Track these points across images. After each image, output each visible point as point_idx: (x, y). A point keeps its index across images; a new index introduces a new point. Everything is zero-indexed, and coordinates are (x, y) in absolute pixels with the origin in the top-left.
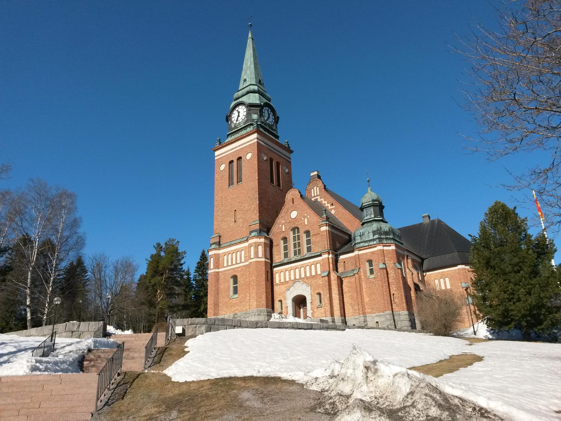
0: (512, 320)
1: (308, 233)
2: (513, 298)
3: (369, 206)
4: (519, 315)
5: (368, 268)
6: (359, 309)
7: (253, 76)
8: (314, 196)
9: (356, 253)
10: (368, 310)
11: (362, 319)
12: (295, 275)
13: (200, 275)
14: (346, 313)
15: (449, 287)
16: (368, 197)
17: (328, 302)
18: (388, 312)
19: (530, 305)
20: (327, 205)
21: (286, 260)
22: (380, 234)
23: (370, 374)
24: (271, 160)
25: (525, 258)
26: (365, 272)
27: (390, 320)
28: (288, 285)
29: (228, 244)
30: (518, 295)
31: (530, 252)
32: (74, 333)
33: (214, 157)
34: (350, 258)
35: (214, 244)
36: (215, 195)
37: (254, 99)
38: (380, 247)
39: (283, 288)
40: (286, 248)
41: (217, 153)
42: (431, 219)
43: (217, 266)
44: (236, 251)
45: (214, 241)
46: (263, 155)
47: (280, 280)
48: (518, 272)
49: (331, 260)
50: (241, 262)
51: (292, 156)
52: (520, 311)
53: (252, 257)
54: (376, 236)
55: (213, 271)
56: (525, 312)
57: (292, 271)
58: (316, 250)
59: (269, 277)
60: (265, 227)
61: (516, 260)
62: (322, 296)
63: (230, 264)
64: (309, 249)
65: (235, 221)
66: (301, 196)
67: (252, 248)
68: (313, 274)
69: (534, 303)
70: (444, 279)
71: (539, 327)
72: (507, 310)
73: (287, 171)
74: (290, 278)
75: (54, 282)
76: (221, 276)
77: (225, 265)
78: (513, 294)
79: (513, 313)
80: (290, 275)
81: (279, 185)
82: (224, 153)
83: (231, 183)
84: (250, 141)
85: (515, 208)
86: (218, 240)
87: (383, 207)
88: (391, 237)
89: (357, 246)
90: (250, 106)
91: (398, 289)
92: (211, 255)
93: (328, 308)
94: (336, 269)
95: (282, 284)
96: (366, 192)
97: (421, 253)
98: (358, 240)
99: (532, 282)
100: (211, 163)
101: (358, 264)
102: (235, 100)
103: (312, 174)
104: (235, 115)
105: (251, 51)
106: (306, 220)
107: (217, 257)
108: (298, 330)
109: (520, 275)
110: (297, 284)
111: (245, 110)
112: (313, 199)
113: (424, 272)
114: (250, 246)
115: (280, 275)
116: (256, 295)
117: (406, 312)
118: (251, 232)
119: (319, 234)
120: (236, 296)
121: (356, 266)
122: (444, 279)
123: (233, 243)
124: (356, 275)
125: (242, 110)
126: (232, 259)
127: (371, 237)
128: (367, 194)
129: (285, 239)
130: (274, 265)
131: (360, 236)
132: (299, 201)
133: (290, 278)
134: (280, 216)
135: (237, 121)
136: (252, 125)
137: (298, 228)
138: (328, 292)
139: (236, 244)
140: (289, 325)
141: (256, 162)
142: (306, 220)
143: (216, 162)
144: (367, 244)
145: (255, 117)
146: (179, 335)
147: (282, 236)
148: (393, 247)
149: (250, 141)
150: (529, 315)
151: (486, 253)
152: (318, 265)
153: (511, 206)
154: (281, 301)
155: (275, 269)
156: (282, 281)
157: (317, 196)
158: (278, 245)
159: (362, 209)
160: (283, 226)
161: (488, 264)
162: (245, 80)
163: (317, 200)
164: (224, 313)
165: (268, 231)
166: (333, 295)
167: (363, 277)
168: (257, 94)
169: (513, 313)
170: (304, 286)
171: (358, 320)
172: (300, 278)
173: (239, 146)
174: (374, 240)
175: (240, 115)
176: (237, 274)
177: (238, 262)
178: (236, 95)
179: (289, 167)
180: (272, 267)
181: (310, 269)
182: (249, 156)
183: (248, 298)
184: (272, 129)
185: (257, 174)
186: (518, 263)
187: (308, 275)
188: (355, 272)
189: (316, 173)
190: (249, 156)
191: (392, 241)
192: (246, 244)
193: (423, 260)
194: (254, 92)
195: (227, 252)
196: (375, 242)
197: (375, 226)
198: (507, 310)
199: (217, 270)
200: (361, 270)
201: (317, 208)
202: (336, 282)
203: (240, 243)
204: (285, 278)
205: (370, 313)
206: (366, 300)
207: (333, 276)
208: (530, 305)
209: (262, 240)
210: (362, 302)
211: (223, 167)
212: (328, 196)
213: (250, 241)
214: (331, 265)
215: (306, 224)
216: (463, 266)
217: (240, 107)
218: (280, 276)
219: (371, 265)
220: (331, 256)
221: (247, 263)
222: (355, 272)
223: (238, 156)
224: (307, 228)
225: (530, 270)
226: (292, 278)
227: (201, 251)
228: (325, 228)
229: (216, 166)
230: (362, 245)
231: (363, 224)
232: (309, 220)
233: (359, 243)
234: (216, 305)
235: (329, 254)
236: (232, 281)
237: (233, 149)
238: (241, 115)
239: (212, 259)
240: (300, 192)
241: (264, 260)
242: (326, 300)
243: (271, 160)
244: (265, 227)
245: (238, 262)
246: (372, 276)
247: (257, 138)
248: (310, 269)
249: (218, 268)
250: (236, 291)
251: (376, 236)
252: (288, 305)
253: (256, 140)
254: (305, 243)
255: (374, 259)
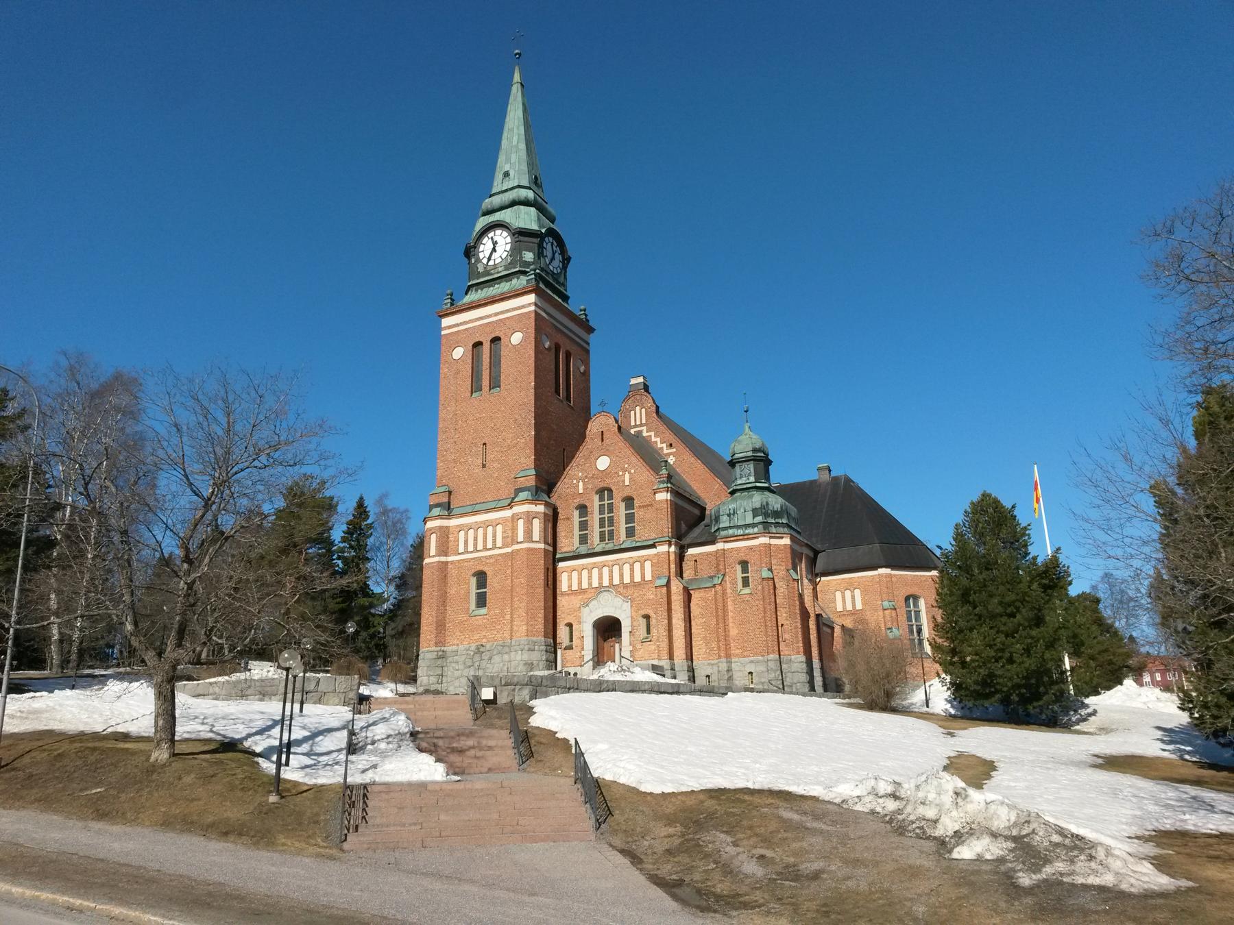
0: (997, 691)
1: (629, 501)
2: (1001, 658)
3: (747, 460)
4: (1009, 684)
5: (739, 575)
6: (719, 648)
7: (524, 167)
8: (636, 426)
9: (720, 546)
10: (734, 651)
11: (723, 666)
12: (600, 578)
13: (351, 547)
14: (695, 653)
15: (859, 606)
16: (744, 444)
17: (666, 633)
18: (771, 657)
19: (1027, 670)
20: (659, 445)
21: (583, 550)
22: (766, 515)
23: (959, 800)
24: (557, 348)
25: (1025, 594)
26: (734, 583)
27: (775, 671)
28: (586, 596)
29: (469, 509)
30: (1011, 653)
31: (1035, 586)
32: (310, 695)
33: (440, 329)
34: (708, 554)
35: (437, 505)
36: (441, 407)
37: (527, 218)
38: (764, 540)
39: (576, 601)
40: (583, 526)
41: (446, 322)
42: (833, 474)
43: (444, 550)
44: (486, 525)
45: (437, 501)
46: (544, 337)
47: (570, 586)
48: (1012, 615)
49: (672, 557)
50: (495, 547)
51: (592, 338)
52: (1011, 679)
53: (520, 538)
54: (759, 519)
55: (436, 559)
56: (1018, 681)
57: (595, 571)
58: (643, 535)
59: (551, 579)
60: (546, 484)
61: (1011, 597)
62: (653, 622)
63: (471, 548)
64: (630, 532)
65: (484, 466)
66: (619, 428)
67: (521, 522)
68: (638, 578)
69: (1033, 667)
70: (852, 592)
71: (1035, 704)
72: (991, 675)
73: (582, 369)
74: (590, 584)
75: (28, 542)
76: (452, 571)
77: (461, 549)
78: (1002, 650)
79: (1001, 681)
80: (590, 578)
81: (568, 398)
82: (461, 324)
83: (476, 387)
84: (519, 308)
85: (1013, 507)
86: (446, 500)
87: (770, 462)
88: (784, 521)
89: (723, 533)
90: (520, 235)
91: (791, 616)
92: (431, 529)
93: (665, 644)
94: (680, 574)
95: (574, 593)
96: (742, 432)
97: (814, 539)
98: (725, 521)
99: (1034, 633)
100: (433, 343)
101: (721, 567)
102: (485, 214)
103: (633, 381)
104: (485, 247)
105: (520, 113)
106: (627, 476)
107: (444, 533)
108: (654, 696)
109: (1015, 620)
110: (605, 597)
111: (509, 239)
112: (632, 431)
113: (817, 575)
114: (515, 518)
115: (570, 576)
116: (527, 613)
117: (802, 658)
118: (518, 491)
119: (651, 505)
120: (483, 611)
121: (719, 571)
122: (852, 592)
123: (478, 507)
124: (719, 588)
125: (503, 240)
126: (476, 539)
127: (749, 520)
128: (743, 437)
129: (583, 509)
130: (558, 556)
131: (729, 515)
132: (613, 437)
133: (590, 584)
134: (574, 463)
135: (489, 259)
136: (524, 273)
137: (610, 490)
138: (665, 614)
139: (486, 511)
140: (647, 687)
141: (532, 353)
142: (627, 476)
143: (443, 341)
144: (740, 532)
145: (529, 256)
146: (487, 702)
147: (577, 501)
148: (786, 541)
149: (519, 308)
150: (1025, 686)
151: (964, 581)
152: (648, 564)
153: (1007, 503)
154: (570, 625)
155: (561, 565)
156: (575, 587)
157: (642, 425)
158: (568, 519)
159: (732, 464)
160: (581, 484)
161: (965, 596)
162: (507, 174)
163: (640, 432)
164: (456, 642)
165: (549, 492)
166: (674, 621)
167: (729, 591)
168: (533, 209)
169: (1001, 681)
170: (619, 601)
171: (715, 668)
172: (611, 585)
173: (496, 314)
174: (754, 525)
175: (496, 249)
176: (485, 569)
177: (489, 545)
178: (488, 203)
179: (587, 365)
180: (555, 561)
181: (632, 570)
182: (516, 338)
183: (508, 617)
184: (558, 283)
185: (532, 377)
186: (1014, 602)
187: (627, 580)
188: (716, 581)
189: (641, 380)
190: (516, 338)
191: (786, 530)
192: (508, 513)
193: (816, 553)
194: (526, 203)
195: (467, 525)
196: (756, 530)
197: (757, 499)
198: (991, 675)
199: (443, 559)
200: (727, 578)
201: (652, 459)
202: (681, 597)
203: (495, 509)
204: (580, 583)
205: (737, 656)
206: (733, 632)
207: (676, 587)
208: (1027, 670)
209: (541, 508)
210: (726, 636)
211: (458, 353)
212: (663, 428)
213: (517, 509)
214: (673, 566)
215: (627, 483)
216: (888, 571)
217: (498, 232)
218: (570, 579)
219: (745, 570)
220: (673, 549)
221: (509, 550)
222: (716, 581)
223: (493, 336)
224: (628, 493)
225: (1031, 615)
226: (595, 584)
227: (357, 499)
228: (664, 496)
229: (443, 348)
230: (731, 532)
231: (732, 493)
232: (631, 476)
233: (725, 529)
234: (441, 626)
235: (670, 545)
236: (474, 581)
237: (481, 318)
238: (499, 249)
239: (434, 537)
240: (617, 422)
241: (542, 546)
242: (659, 630)
243: (557, 348)
244: (546, 484)
245: (489, 545)
246: (747, 591)
247: (536, 304)
248: (632, 570)
249: (446, 555)
250: (481, 601)
251: (759, 519)
252: (584, 634)
253: (533, 308)
254: (623, 519)
255: (753, 559)
